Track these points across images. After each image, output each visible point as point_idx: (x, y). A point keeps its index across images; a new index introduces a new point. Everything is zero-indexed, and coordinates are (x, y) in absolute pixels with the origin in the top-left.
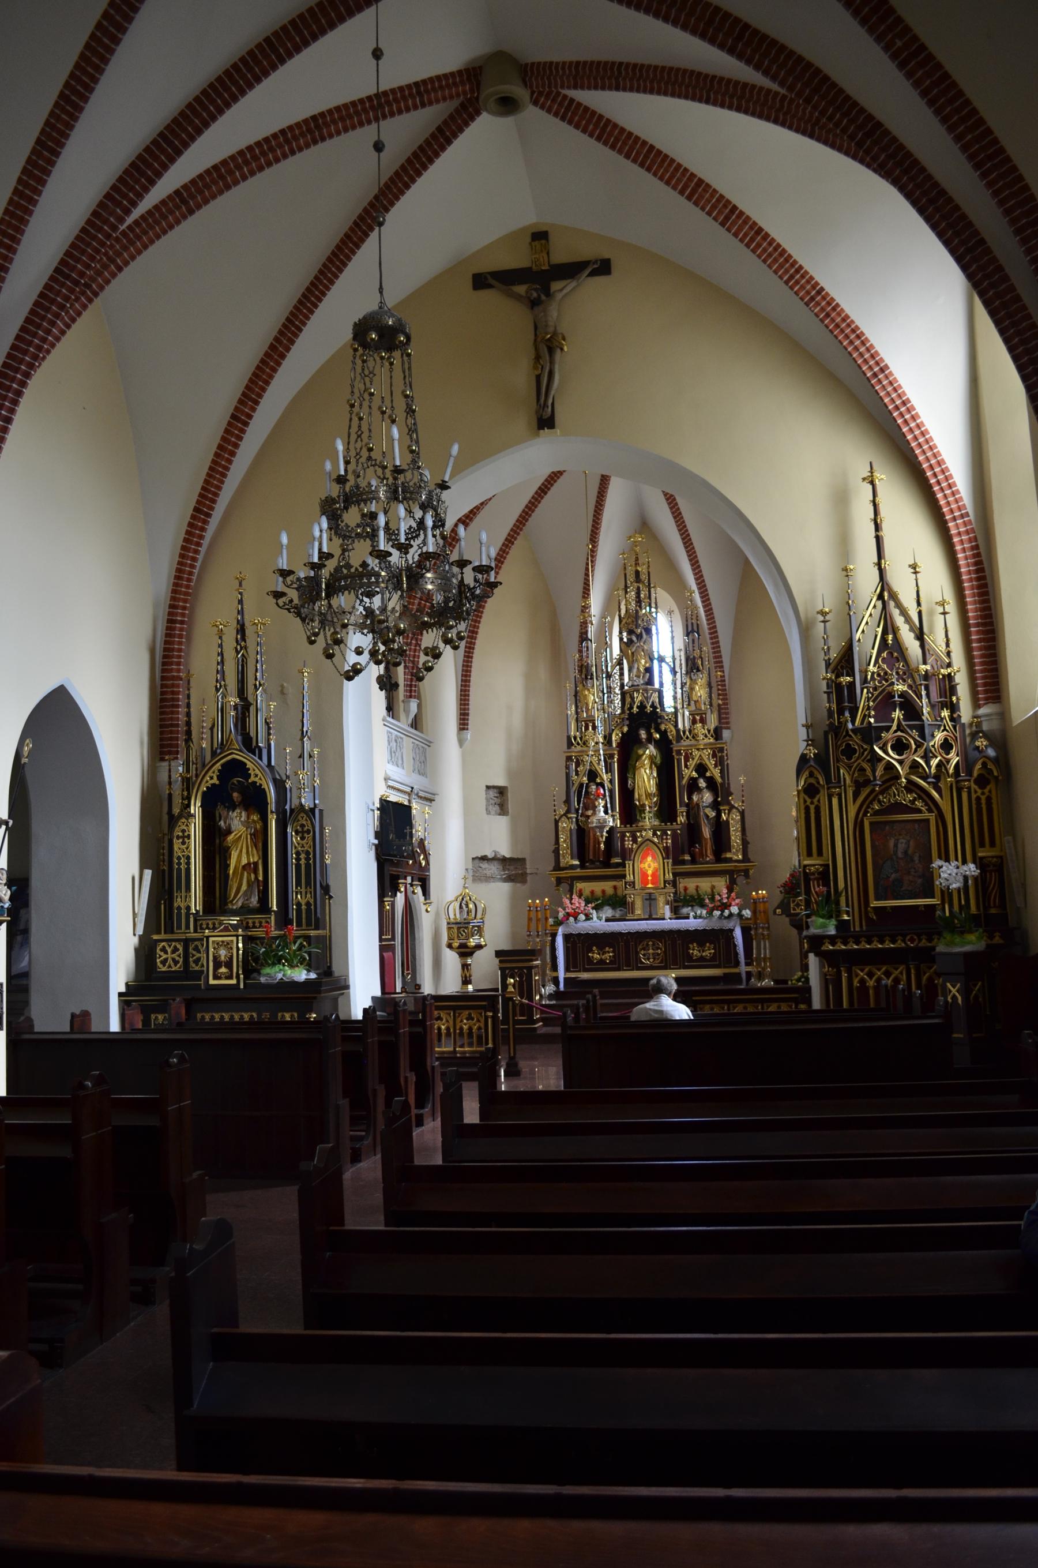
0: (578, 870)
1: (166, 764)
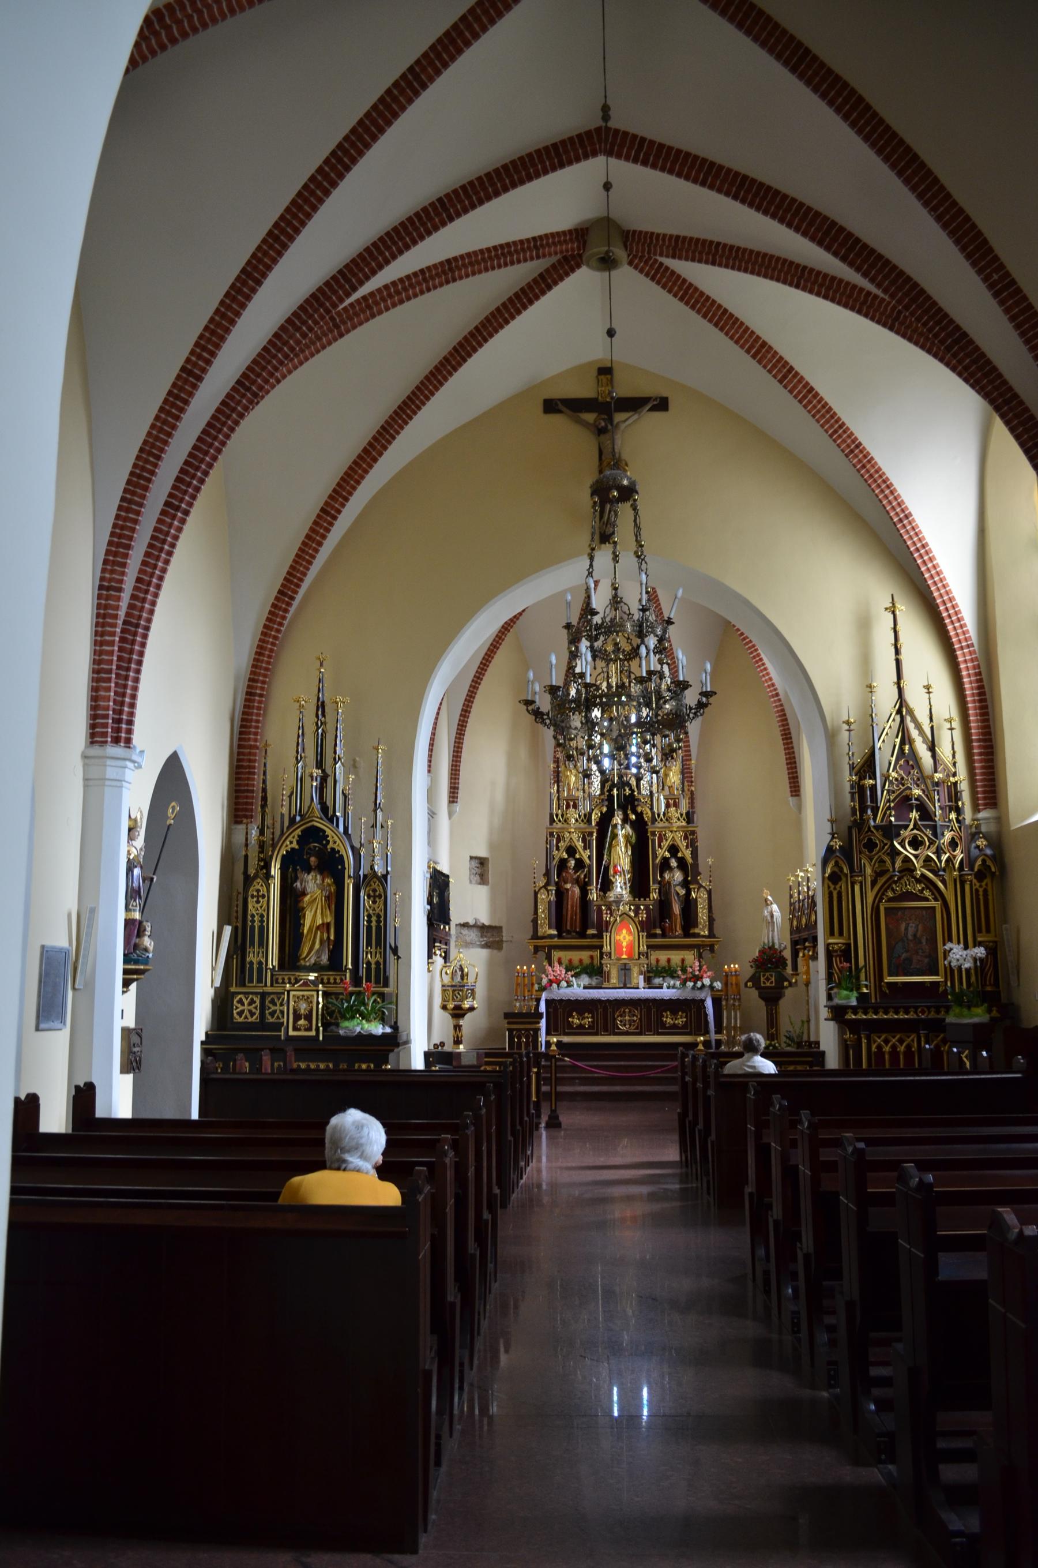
0: (556, 939)
1: (242, 827)
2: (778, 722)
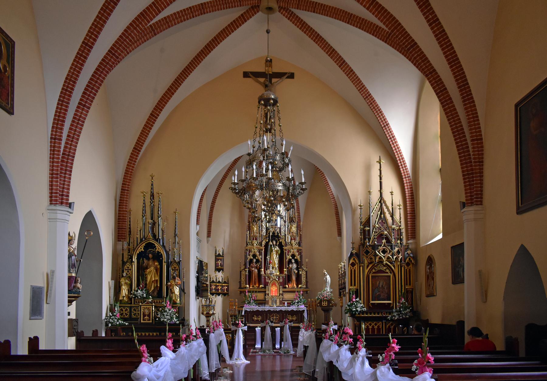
2: (334, 208)
